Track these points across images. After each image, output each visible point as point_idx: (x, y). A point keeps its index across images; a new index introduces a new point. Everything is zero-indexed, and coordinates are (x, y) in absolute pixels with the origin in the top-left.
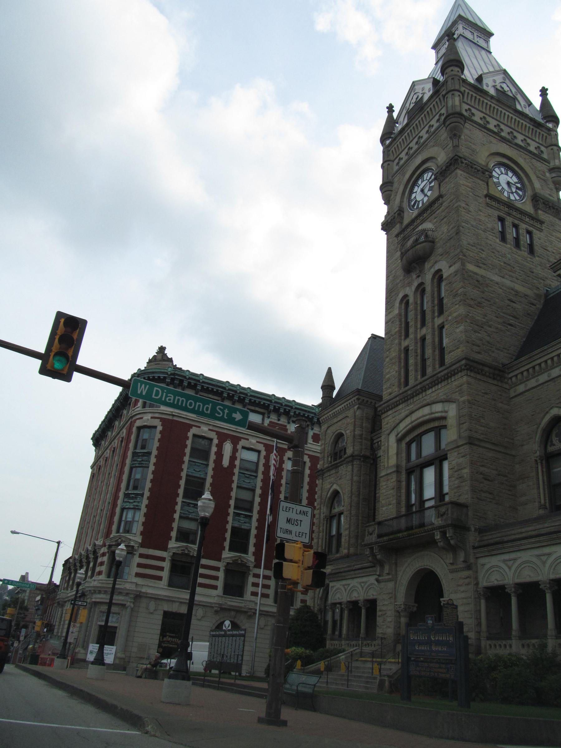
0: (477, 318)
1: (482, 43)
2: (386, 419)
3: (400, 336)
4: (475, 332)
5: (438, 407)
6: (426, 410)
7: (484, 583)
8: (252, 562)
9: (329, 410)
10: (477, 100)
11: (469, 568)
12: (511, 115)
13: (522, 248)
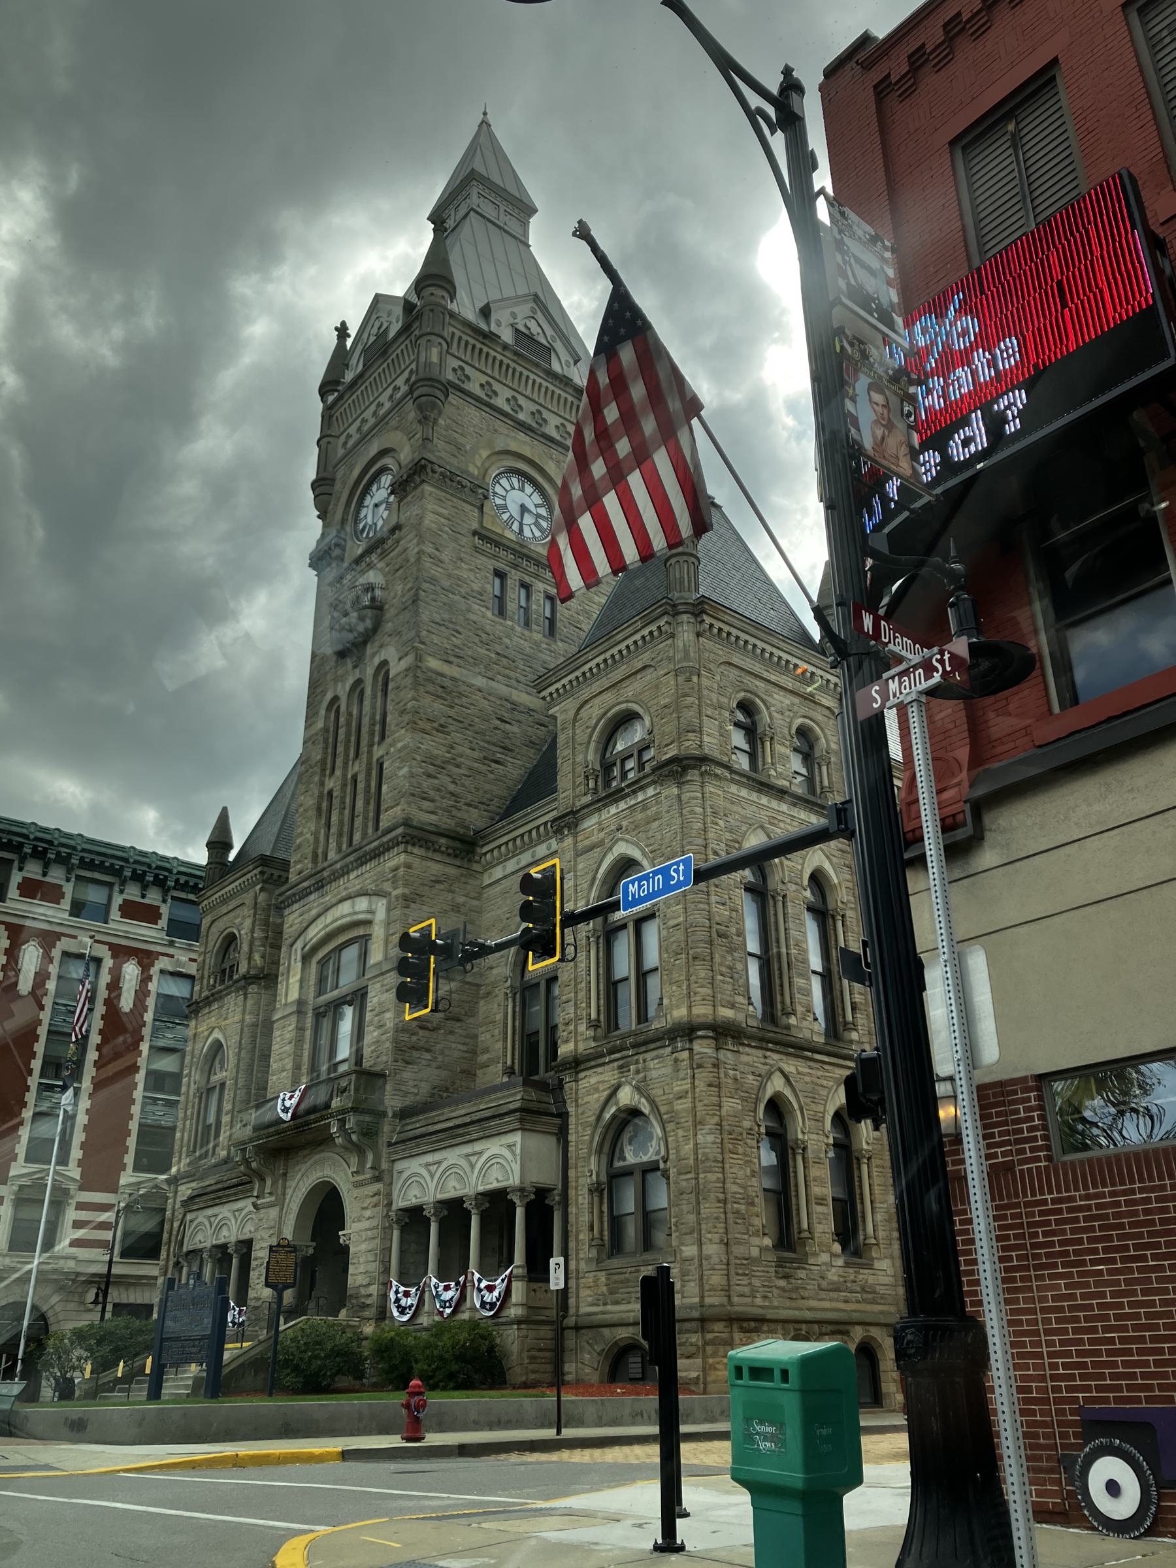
0: (436, 752)
1: (513, 226)
2: (292, 917)
3: (323, 770)
4: (430, 776)
5: (362, 904)
6: (345, 908)
7: (400, 1203)
8: (74, 1180)
9: (216, 889)
10: (477, 351)
11: (377, 1179)
12: (539, 380)
13: (534, 627)
